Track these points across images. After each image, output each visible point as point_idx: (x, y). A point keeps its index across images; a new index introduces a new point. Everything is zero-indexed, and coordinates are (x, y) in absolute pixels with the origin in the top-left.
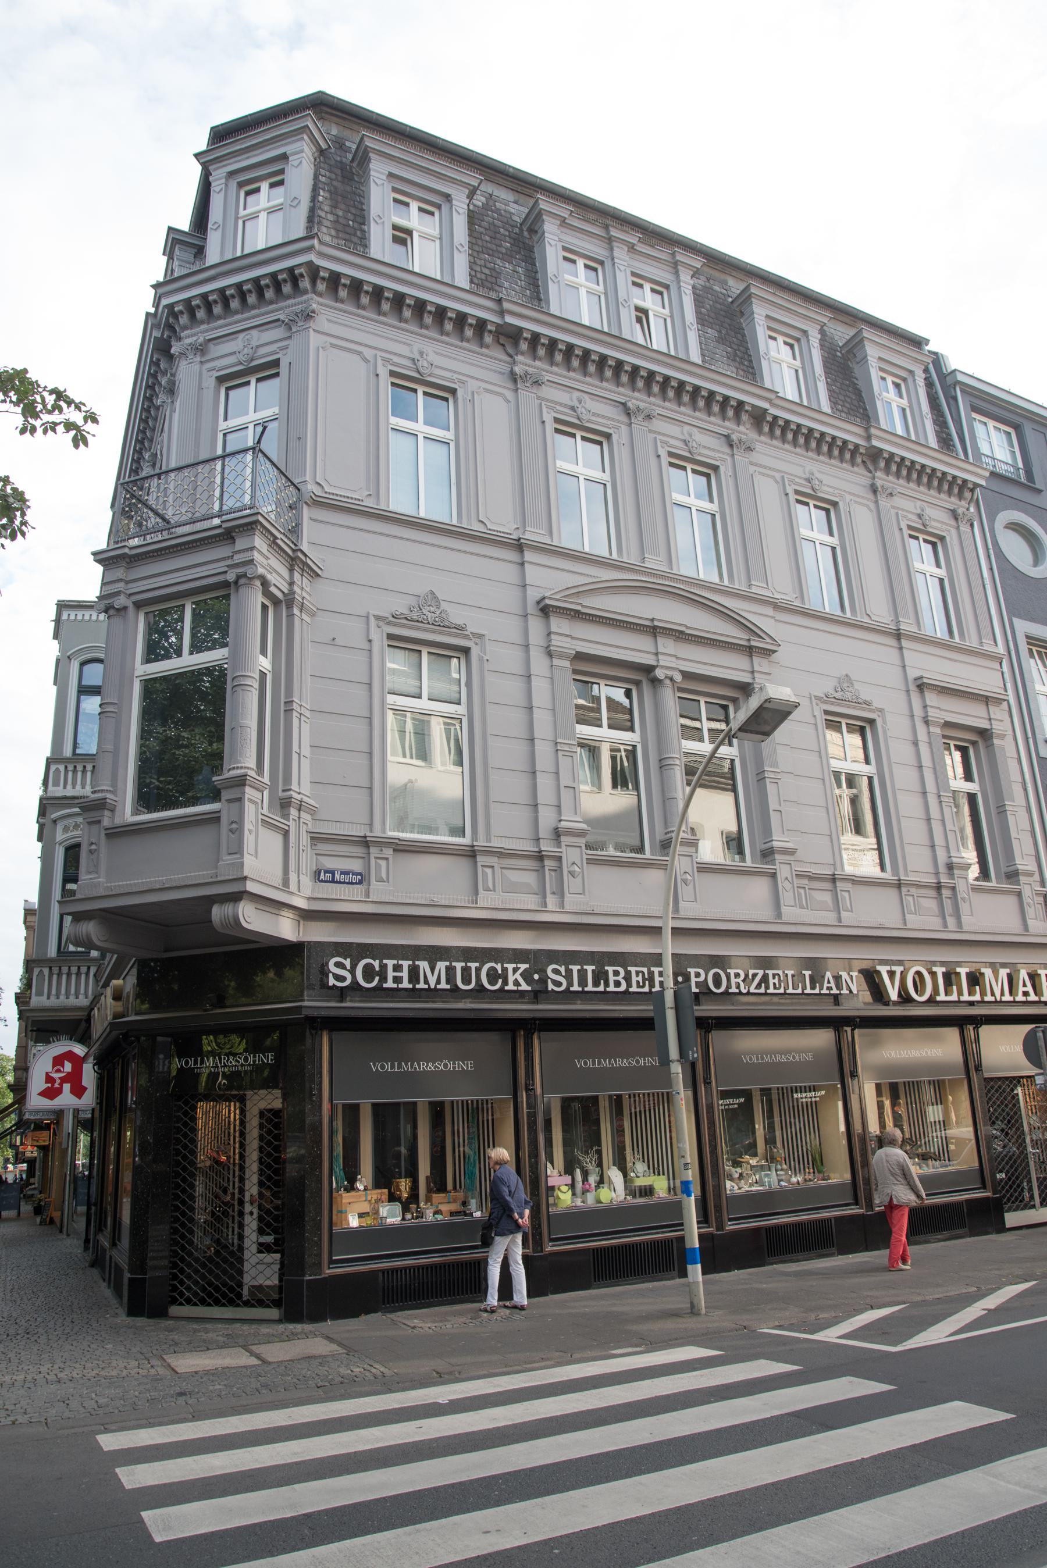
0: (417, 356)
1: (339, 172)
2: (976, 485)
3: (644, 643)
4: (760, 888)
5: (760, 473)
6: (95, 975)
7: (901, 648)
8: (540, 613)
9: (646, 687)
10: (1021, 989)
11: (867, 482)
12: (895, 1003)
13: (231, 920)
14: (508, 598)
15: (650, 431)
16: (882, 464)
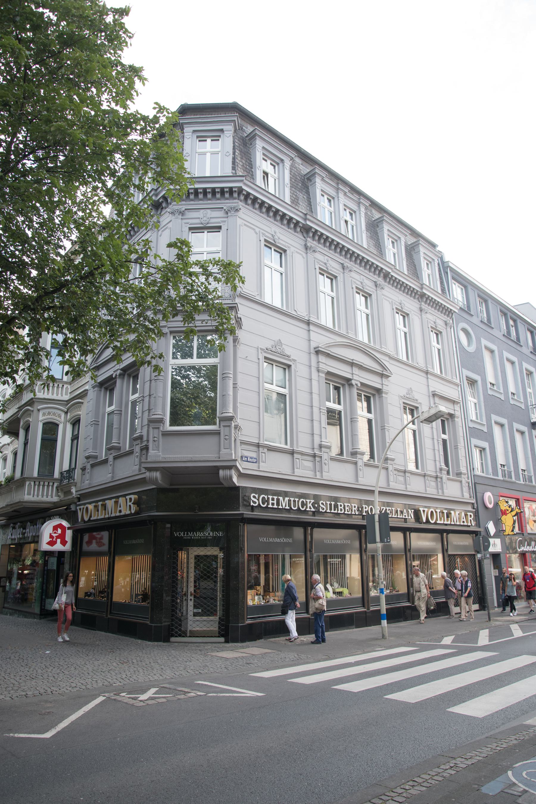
0: (273, 233)
1: (241, 141)
2: (454, 312)
3: (347, 368)
4: (350, 468)
5: (385, 299)
6: (57, 487)
7: (428, 378)
8: (315, 353)
9: (347, 387)
10: (462, 520)
11: (418, 306)
12: (424, 523)
13: (228, 477)
14: (303, 345)
15: (351, 277)
16: (311, 235)
